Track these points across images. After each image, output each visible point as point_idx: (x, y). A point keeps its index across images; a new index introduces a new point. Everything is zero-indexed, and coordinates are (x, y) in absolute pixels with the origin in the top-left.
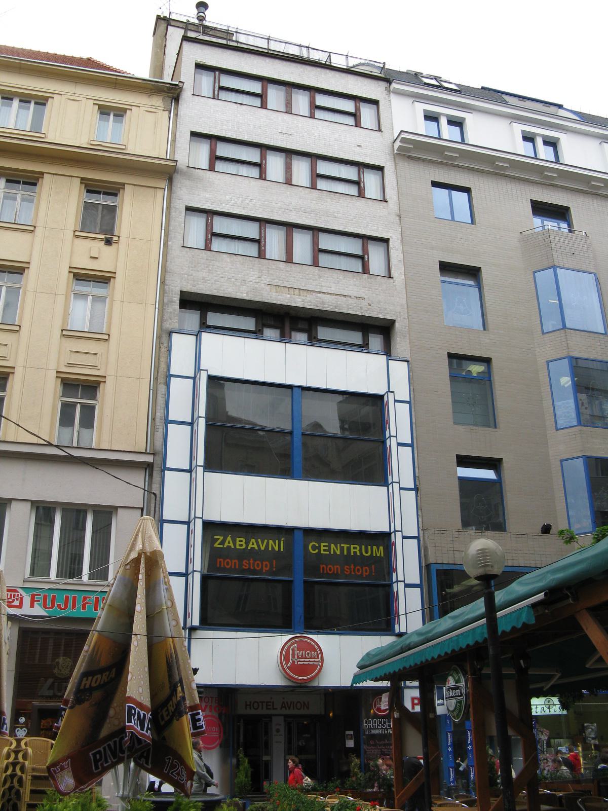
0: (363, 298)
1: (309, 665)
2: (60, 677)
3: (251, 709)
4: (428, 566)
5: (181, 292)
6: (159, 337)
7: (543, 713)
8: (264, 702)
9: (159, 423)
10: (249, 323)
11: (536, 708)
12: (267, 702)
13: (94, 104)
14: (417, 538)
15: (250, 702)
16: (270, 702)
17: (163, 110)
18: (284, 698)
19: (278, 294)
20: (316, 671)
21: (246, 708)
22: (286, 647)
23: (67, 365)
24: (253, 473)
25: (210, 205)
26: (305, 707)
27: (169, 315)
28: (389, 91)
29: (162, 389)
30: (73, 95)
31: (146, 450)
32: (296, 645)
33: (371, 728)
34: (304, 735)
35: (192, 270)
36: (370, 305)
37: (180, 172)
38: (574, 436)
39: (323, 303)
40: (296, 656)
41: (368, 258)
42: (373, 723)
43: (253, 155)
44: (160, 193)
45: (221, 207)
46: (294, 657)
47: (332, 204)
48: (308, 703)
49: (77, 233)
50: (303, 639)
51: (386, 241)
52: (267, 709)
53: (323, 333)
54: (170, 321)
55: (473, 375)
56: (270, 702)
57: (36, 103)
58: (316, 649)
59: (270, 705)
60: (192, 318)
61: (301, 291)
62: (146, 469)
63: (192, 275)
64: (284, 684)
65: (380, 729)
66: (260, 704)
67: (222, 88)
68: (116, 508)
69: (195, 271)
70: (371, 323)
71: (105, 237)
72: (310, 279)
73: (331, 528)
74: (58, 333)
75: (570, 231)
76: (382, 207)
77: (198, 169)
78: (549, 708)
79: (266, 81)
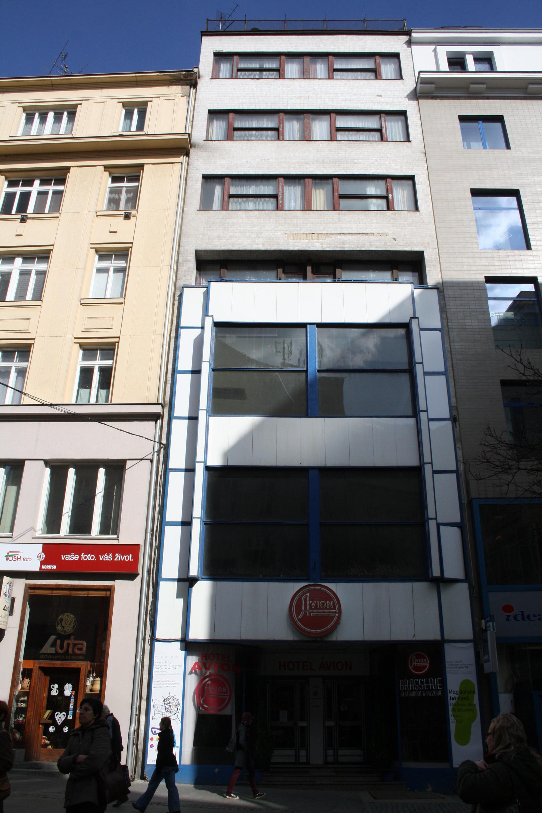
1: (323, 616)
2: (63, 634)
4: (470, 502)
5: (197, 251)
13: (119, 102)
14: (456, 472)
17: (182, 96)
19: (295, 241)
20: (332, 623)
22: (297, 598)
23: (84, 330)
25: (225, 170)
30: (99, 98)
32: (308, 594)
33: (432, 689)
35: (207, 230)
37: (197, 147)
39: (344, 243)
40: (308, 607)
41: (392, 197)
42: (404, 685)
45: (237, 170)
46: (306, 608)
47: (352, 151)
51: (411, 178)
54: (184, 278)
55: (380, 190)
58: (332, 598)
64: (296, 639)
65: (417, 691)
69: (210, 230)
71: (125, 213)
72: (330, 223)
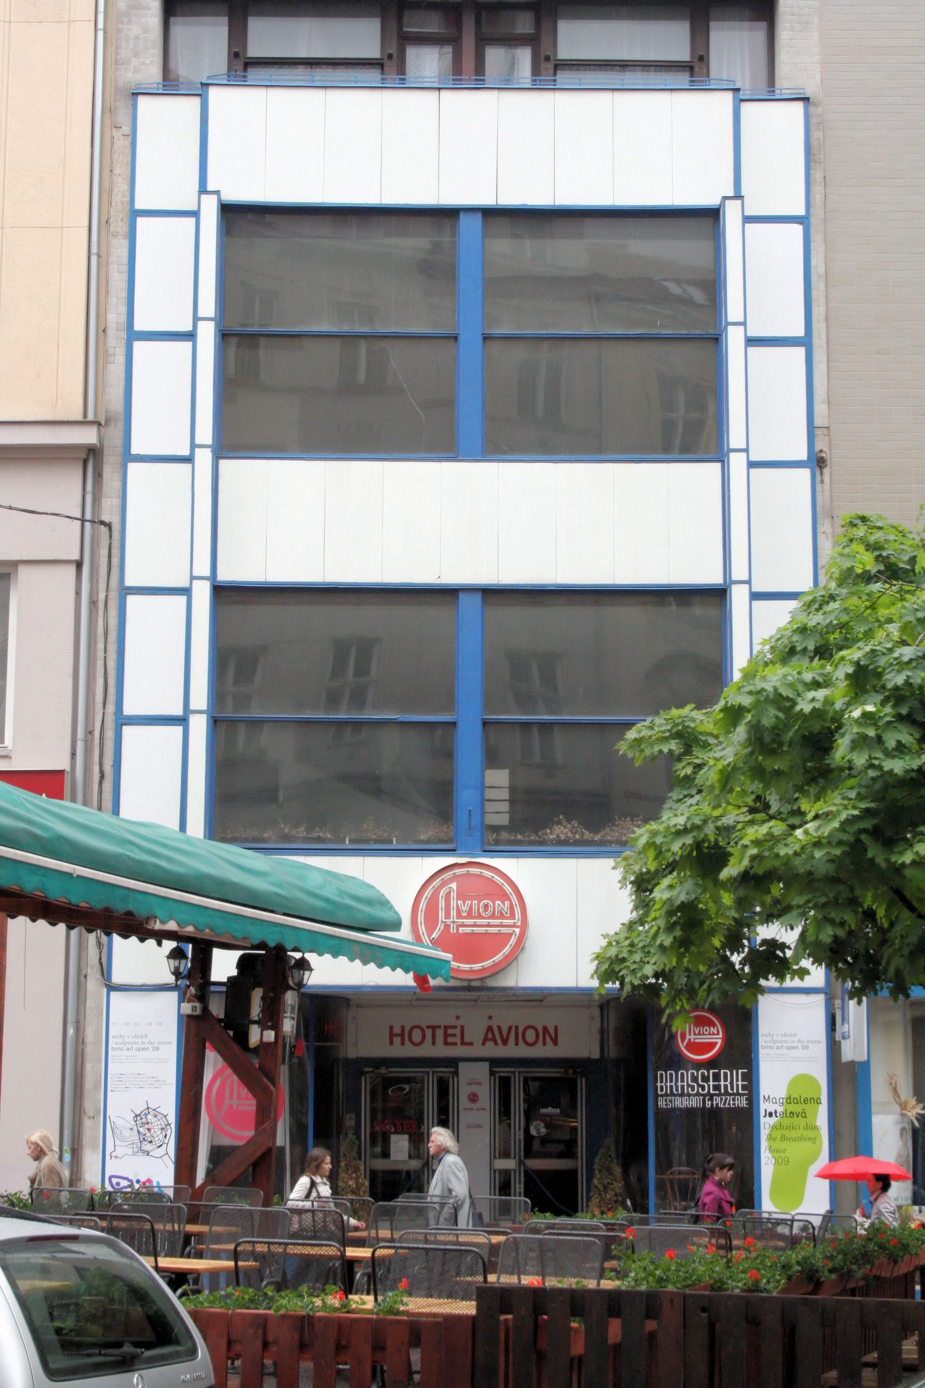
1: (486, 934)
3: (403, 1043)
8: (439, 1027)
9: (115, 340)
12: (446, 1028)
15: (403, 1028)
16: (455, 1027)
18: (458, 1018)
21: (391, 1043)
22: (428, 893)
26: (548, 1039)
27: (131, 45)
29: (120, 249)
31: (85, 414)
32: (454, 885)
33: (672, 1094)
34: (544, 1111)
40: (453, 913)
42: (666, 1082)
46: (448, 915)
48: (556, 1028)
50: (474, 870)
52: (446, 1043)
56: (455, 1027)
59: (454, 1035)
62: (85, 462)
66: (429, 1033)
68: (15, 564)
73: (617, 582)
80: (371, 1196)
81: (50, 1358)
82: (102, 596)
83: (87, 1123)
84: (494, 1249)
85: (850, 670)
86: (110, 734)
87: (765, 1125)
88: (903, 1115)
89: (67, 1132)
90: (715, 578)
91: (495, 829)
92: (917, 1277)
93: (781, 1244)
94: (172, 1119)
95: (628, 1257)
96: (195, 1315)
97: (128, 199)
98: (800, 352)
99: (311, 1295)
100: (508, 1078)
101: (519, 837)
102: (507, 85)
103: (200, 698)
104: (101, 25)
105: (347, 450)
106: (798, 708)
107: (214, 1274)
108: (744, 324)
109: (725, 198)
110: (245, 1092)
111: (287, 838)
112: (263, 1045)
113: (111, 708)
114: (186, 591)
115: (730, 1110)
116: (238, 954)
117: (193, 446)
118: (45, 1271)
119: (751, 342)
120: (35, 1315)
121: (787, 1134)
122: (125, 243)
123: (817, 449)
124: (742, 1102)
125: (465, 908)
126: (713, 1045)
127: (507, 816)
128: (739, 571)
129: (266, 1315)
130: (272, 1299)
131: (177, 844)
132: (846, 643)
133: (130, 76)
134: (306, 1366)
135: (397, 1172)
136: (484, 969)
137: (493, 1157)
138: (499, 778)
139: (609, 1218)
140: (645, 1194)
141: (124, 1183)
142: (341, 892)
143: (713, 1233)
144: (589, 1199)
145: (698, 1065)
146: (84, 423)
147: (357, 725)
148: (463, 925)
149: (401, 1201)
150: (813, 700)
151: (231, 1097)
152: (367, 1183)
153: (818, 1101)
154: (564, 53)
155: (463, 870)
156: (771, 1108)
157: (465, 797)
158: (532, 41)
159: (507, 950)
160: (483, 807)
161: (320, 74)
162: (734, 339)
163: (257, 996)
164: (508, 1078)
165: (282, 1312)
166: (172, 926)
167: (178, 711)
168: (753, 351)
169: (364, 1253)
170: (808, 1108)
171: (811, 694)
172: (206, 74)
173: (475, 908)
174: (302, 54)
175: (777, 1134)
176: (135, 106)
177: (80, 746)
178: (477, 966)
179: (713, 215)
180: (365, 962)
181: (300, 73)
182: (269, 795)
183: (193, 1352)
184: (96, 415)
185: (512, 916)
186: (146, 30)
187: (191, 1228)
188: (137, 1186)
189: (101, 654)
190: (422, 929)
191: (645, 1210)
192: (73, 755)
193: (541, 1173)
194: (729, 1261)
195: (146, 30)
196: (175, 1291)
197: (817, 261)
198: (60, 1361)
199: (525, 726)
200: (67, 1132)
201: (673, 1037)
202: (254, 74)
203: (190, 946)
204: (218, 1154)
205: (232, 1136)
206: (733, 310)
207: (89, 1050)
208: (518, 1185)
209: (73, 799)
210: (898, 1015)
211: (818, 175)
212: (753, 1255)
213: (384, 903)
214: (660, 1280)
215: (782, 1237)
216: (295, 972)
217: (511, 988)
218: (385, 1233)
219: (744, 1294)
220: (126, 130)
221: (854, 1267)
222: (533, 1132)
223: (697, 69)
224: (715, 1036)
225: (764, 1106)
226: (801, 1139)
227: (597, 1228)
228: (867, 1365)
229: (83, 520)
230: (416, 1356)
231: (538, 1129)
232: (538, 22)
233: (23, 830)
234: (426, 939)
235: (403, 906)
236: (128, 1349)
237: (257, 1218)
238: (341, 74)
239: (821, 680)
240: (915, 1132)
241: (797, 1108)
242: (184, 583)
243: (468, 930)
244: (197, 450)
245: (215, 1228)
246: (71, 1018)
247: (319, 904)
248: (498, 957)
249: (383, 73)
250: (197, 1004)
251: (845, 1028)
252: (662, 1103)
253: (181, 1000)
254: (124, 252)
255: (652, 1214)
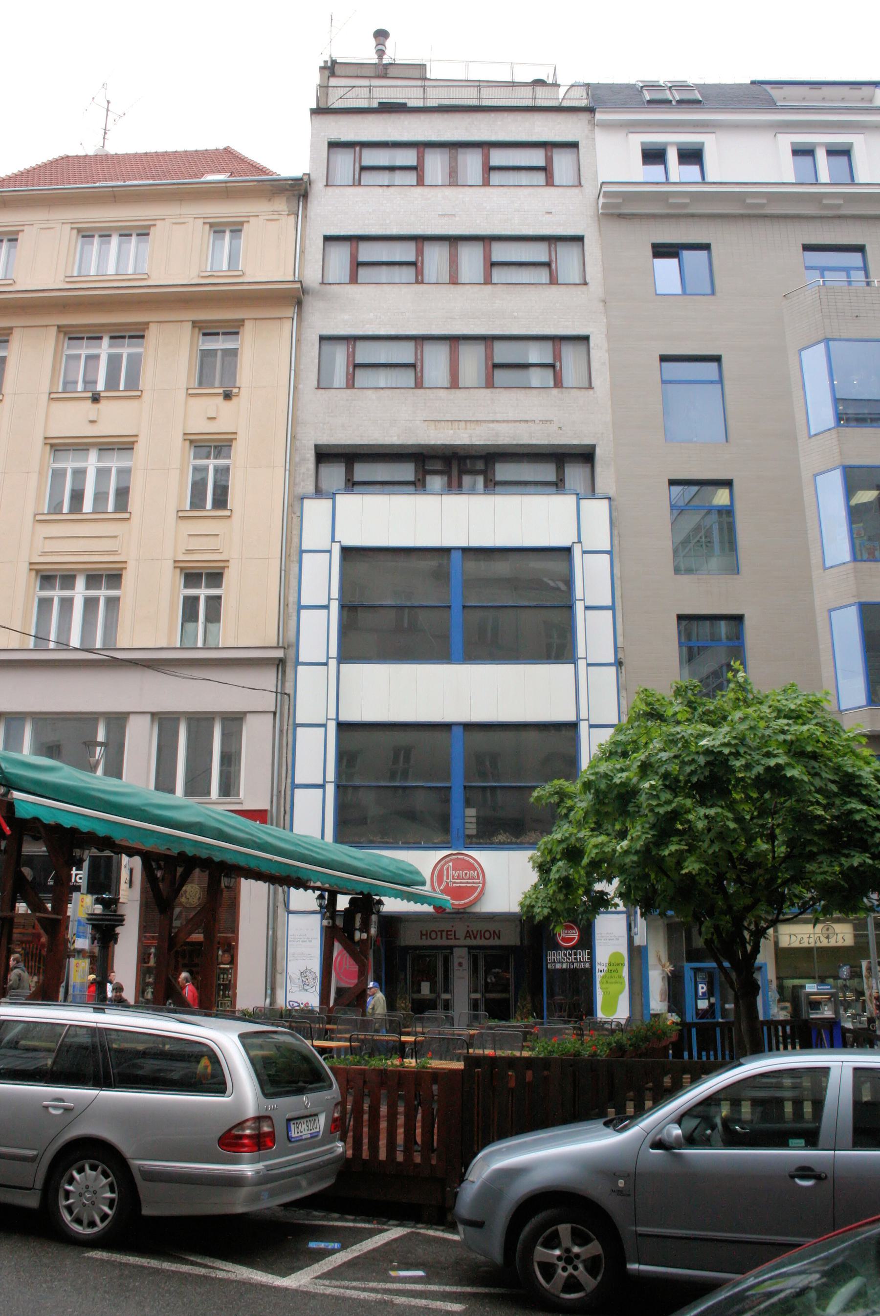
0: (551, 421)
1: (466, 886)
3: (427, 939)
6: (290, 505)
7: (818, 944)
10: (407, 471)
11: (809, 937)
12: (447, 931)
13: (204, 223)
15: (427, 931)
21: (421, 938)
24: (408, 660)
28: (593, 124)
32: (451, 864)
33: (554, 962)
34: (494, 970)
36: (560, 428)
38: (845, 577)
40: (450, 877)
43: (406, 252)
44: (287, 324)
46: (448, 878)
48: (499, 931)
49: (190, 391)
52: (447, 938)
53: (503, 471)
57: (232, 231)
58: (471, 866)
59: (451, 935)
60: (335, 474)
61: (468, 424)
63: (328, 423)
67: (363, 169)
70: (567, 451)
74: (29, 518)
75: (868, 284)
76: (579, 293)
77: (333, 284)
78: (828, 937)
79: (422, 146)
80: (412, 1011)
81: (265, 1088)
82: (285, 728)
83: (278, 976)
84: (472, 1036)
85: (639, 763)
86: (289, 793)
87: (599, 976)
88: (663, 971)
89: (269, 980)
90: (572, 718)
91: (469, 836)
92: (670, 1047)
93: (607, 1033)
94: (318, 974)
95: (535, 1041)
96: (331, 1068)
97: (299, 545)
98: (610, 612)
99: (386, 1059)
100: (477, 955)
101: (481, 841)
102: (472, 492)
103: (331, 775)
104: (287, 468)
105: (399, 660)
106: (614, 781)
107: (339, 1049)
108: (583, 600)
109: (574, 543)
110: (352, 962)
111: (371, 842)
112: (361, 940)
113: (289, 780)
114: (324, 726)
115: (582, 969)
116: (349, 897)
117: (328, 658)
118: (261, 1047)
119: (587, 608)
120: (258, 1067)
121: (610, 980)
122: (297, 565)
123: (619, 657)
124: (588, 966)
125: (456, 875)
126: (574, 938)
127: (475, 830)
128: (583, 715)
129: (364, 1069)
130: (368, 1062)
131: (320, 845)
132: (636, 750)
133: (300, 490)
134: (383, 1092)
135: (424, 1000)
136: (465, 904)
137: (470, 992)
138: (472, 812)
139: (526, 1022)
140: (542, 1011)
141: (296, 1004)
142: (398, 868)
143: (574, 1028)
144: (515, 1012)
145: (566, 948)
146: (277, 647)
147: (404, 788)
148: (455, 883)
149: (426, 1015)
150: (621, 777)
151: (346, 964)
152: (410, 1005)
153: (623, 965)
154: (499, 477)
155: (456, 857)
156: (601, 968)
157: (456, 823)
158: (484, 472)
159: (476, 894)
160: (464, 825)
161: (387, 488)
162: (579, 607)
163: (358, 917)
164: (477, 955)
165: (373, 1067)
166: (318, 884)
167: (321, 782)
168: (589, 612)
169: (411, 1039)
170: (618, 968)
171: (619, 775)
172: (335, 489)
173: (460, 875)
174: (379, 479)
175: (605, 980)
176: (302, 504)
177: (275, 798)
178: (462, 902)
179: (567, 551)
180: (409, 901)
181: (378, 487)
182: (363, 821)
183: (331, 1086)
184: (283, 643)
185: (478, 878)
186: (308, 470)
187: (328, 1026)
188: (302, 1006)
189: (284, 755)
190: (436, 885)
191: (542, 1018)
192: (272, 802)
193: (494, 1000)
194: (583, 1042)
195: (308, 470)
196: (321, 1056)
197: (617, 571)
198: (270, 1090)
199: (484, 788)
200: (269, 980)
201: (555, 935)
202: (356, 488)
203: (327, 893)
204: (339, 991)
205: (347, 982)
206: (579, 593)
207: (279, 941)
208: (482, 1006)
209: (272, 824)
210: (660, 923)
211: (616, 533)
212: (594, 1039)
213: (418, 873)
214: (550, 1052)
215: (607, 1030)
216: (376, 906)
217: (477, 913)
218: (419, 1029)
219: (590, 1058)
220: (298, 514)
221: (641, 1044)
222: (489, 980)
223: (559, 485)
224: (575, 935)
225: (598, 967)
226: (616, 982)
227: (520, 1027)
228: (647, 1089)
229: (277, 693)
230: (435, 1088)
231: (491, 979)
232: (486, 465)
233: (250, 839)
234: (438, 890)
235: (427, 874)
236: (301, 1084)
237: (359, 1022)
238: (396, 488)
239: (624, 767)
240: (669, 978)
241: (614, 968)
242: (323, 721)
243: (458, 885)
244: (330, 660)
245: (339, 1027)
246: (270, 926)
247: (388, 873)
248: (472, 898)
249: (416, 487)
250: (330, 921)
251: (636, 930)
252: (550, 966)
253: (322, 919)
254: (296, 569)
255: (545, 1020)
